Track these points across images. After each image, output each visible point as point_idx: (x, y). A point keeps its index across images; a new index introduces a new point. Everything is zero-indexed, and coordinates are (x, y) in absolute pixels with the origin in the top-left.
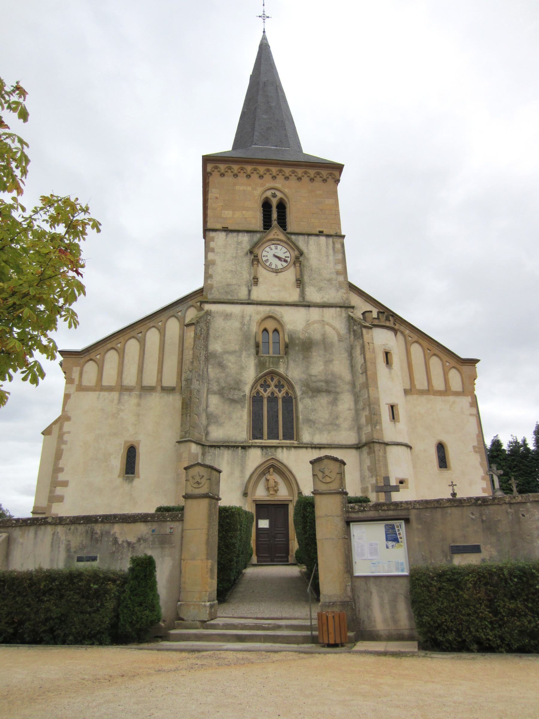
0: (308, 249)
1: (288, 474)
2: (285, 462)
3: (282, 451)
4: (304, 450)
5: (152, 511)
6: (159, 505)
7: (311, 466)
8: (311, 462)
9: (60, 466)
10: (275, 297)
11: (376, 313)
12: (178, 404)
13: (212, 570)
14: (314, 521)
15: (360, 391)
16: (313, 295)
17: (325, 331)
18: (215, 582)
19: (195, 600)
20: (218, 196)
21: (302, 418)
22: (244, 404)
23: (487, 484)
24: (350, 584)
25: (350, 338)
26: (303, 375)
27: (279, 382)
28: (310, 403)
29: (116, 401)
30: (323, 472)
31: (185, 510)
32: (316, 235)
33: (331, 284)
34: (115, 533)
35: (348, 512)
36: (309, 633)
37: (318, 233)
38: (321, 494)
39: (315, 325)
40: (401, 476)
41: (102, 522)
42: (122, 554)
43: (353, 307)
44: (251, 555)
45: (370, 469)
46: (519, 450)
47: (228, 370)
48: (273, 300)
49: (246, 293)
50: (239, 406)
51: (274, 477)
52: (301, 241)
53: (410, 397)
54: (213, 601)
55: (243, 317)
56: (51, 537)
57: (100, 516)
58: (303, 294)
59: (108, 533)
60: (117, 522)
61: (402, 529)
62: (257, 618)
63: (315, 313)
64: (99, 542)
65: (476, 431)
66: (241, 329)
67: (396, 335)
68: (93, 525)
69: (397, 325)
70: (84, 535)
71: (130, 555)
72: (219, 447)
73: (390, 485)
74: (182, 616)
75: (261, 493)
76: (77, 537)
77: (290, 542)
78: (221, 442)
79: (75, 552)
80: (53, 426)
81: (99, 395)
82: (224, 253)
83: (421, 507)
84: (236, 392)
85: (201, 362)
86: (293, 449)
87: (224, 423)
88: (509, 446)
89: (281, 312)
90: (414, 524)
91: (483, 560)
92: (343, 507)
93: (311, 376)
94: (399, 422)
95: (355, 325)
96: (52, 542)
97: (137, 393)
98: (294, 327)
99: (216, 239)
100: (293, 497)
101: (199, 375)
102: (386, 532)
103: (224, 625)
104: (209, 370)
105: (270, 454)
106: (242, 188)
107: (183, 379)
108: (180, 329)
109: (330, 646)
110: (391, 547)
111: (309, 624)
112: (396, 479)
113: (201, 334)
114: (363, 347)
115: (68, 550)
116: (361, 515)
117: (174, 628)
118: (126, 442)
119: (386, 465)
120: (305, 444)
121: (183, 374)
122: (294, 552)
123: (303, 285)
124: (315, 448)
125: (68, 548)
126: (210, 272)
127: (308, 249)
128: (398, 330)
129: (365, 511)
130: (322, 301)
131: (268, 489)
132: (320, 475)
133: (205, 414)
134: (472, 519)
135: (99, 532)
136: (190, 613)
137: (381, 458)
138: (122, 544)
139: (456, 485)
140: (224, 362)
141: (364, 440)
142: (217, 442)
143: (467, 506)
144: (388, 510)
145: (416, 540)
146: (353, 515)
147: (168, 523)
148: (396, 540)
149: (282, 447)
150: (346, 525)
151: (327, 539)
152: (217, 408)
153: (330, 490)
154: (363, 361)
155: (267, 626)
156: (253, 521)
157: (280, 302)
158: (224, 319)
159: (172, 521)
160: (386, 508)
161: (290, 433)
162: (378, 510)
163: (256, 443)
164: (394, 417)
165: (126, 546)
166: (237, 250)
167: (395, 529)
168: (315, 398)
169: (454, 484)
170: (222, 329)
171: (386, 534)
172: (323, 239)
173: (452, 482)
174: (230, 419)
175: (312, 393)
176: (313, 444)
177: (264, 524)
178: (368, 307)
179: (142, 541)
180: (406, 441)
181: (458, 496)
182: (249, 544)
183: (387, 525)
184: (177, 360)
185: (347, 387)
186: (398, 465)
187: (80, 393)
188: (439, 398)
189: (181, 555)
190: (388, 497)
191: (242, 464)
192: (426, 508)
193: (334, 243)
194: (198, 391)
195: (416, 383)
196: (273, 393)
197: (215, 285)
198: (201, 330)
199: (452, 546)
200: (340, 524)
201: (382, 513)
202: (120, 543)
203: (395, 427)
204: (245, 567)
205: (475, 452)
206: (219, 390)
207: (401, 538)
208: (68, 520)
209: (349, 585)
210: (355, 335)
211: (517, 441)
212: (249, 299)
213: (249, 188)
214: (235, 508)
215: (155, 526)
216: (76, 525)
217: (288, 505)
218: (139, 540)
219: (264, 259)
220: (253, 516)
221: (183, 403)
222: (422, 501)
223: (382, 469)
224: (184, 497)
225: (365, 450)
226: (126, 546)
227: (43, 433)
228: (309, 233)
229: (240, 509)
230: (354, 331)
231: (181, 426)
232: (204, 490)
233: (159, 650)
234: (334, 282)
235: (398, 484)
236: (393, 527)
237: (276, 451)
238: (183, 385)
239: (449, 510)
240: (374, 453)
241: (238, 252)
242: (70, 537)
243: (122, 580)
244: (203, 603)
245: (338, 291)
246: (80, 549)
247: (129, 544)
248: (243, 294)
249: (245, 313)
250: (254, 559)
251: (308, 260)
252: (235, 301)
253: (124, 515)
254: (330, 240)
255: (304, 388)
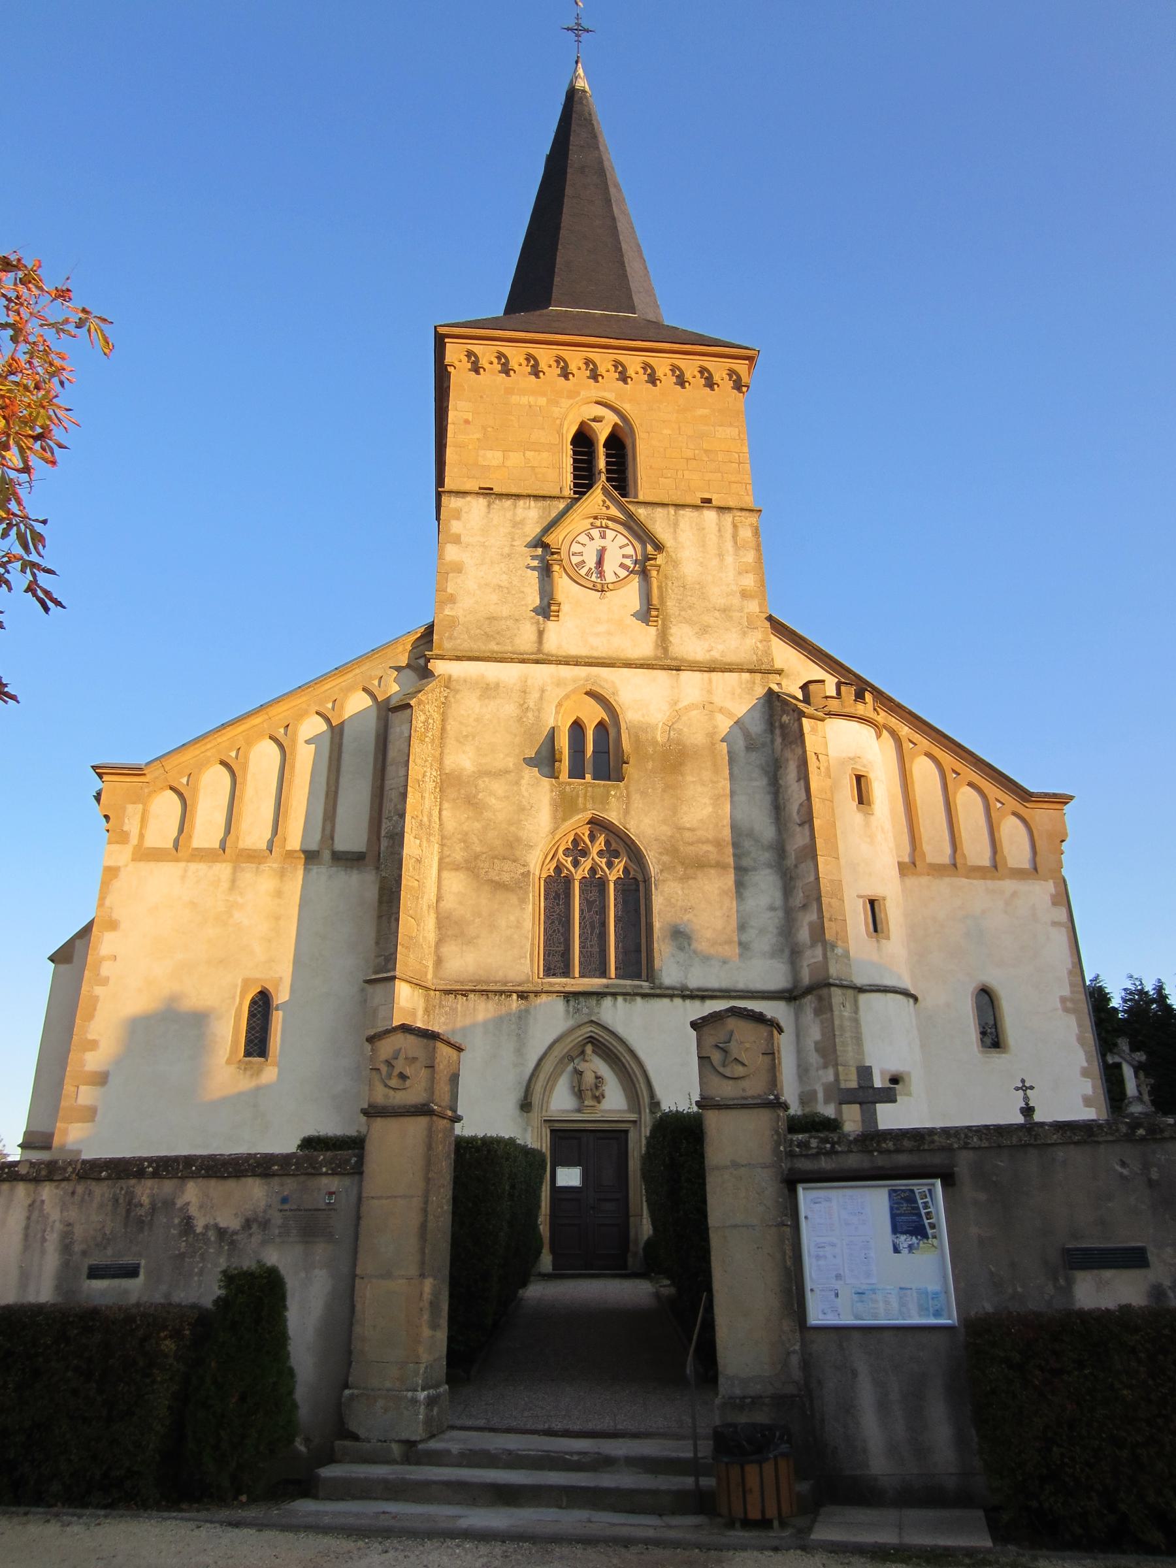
0: (675, 539)
1: (627, 1058)
2: (620, 1030)
3: (615, 1005)
4: (666, 1001)
5: (287, 1144)
6: (310, 1131)
7: (693, 1034)
8: (694, 1025)
9: (90, 1037)
10: (600, 647)
11: (834, 688)
12: (372, 893)
13: (434, 1305)
14: (704, 1179)
15: (796, 866)
16: (686, 643)
17: (715, 727)
18: (442, 1335)
19: (388, 1384)
20: (470, 417)
21: (661, 929)
22: (527, 893)
23: (1094, 1087)
24: (797, 1347)
25: (773, 741)
26: (664, 828)
27: (607, 843)
28: (680, 892)
29: (225, 885)
30: (725, 1051)
31: (369, 1146)
32: (695, 507)
33: (730, 618)
34: (188, 1204)
35: (791, 1155)
36: (688, 1482)
37: (699, 502)
38: (719, 1107)
39: (695, 712)
40: (894, 1067)
41: (155, 1175)
42: (203, 1258)
43: (779, 672)
44: (539, 1253)
45: (821, 1049)
46: (1148, 1009)
47: (487, 814)
48: (595, 654)
49: (533, 637)
50: (514, 899)
51: (598, 1066)
52: (658, 523)
53: (911, 881)
54: (437, 1386)
55: (525, 692)
56: (25, 1214)
57: (151, 1160)
58: (663, 639)
59: (169, 1204)
60: (194, 1176)
61: (935, 1198)
62: (550, 1433)
63: (692, 684)
64: (146, 1228)
65: (1067, 962)
66: (520, 719)
67: (879, 736)
68: (133, 1182)
69: (882, 714)
70: (109, 1208)
71: (223, 1263)
72: (465, 994)
73: (872, 1087)
74: (353, 1426)
75: (561, 1102)
76: (91, 1214)
77: (632, 1219)
78: (471, 981)
79: (84, 1253)
80: (78, 942)
81: (186, 871)
82: (483, 545)
83: (985, 1144)
84: (507, 865)
85: (427, 795)
86: (639, 999)
87: (478, 937)
88: (1125, 1001)
89: (613, 682)
90: (968, 1190)
91: (1157, 1292)
92: (778, 1144)
93: (680, 829)
94: (888, 938)
95: (784, 712)
96: (27, 1228)
97: (275, 865)
98: (643, 716)
99: (464, 516)
100: (640, 1113)
101: (421, 824)
102: (892, 1209)
103: (462, 1454)
104: (444, 813)
105: (585, 1010)
106: (524, 400)
107: (383, 833)
108: (378, 718)
109: (748, 1524)
110: (906, 1251)
111: (690, 1455)
112: (882, 1073)
113: (427, 730)
114: (803, 763)
115: (66, 1247)
116: (825, 1164)
117: (331, 1459)
118: (247, 982)
119: (858, 1039)
120: (668, 988)
121: (384, 821)
122: (642, 1244)
123: (664, 620)
124: (692, 997)
125: (67, 1241)
126: (449, 590)
127: (675, 539)
128: (885, 726)
129: (837, 1153)
130: (708, 657)
131: (579, 1093)
132: (716, 1057)
133: (433, 916)
134: (1121, 1175)
135: (145, 1200)
136: (371, 1421)
137: (847, 1023)
138: (203, 1234)
139: (1032, 1088)
140: (480, 796)
141: (806, 978)
142: (462, 983)
143: (1107, 1142)
144: (898, 1151)
145: (974, 1230)
146: (804, 1165)
147: (325, 1180)
148: (919, 1231)
149: (614, 995)
150: (786, 1191)
151: (735, 1226)
152: (460, 903)
153: (746, 1098)
154: (804, 797)
155: (575, 1458)
156: (545, 1171)
157: (610, 658)
158: (481, 698)
159: (334, 1174)
160: (890, 1145)
161: (637, 961)
162: (871, 1152)
163: (551, 984)
164: (876, 925)
165: (213, 1239)
166: (513, 540)
167: (916, 1202)
168: (690, 882)
169: (1027, 1085)
170: (477, 720)
171: (893, 1217)
172: (710, 515)
173: (1023, 1081)
174: (492, 927)
175: (686, 868)
176: (688, 989)
177: (569, 1177)
178: (815, 672)
179: (255, 1227)
180: (907, 983)
181: (1038, 1117)
182: (535, 1226)
183: (895, 1191)
184: (369, 789)
185: (766, 856)
186: (886, 1041)
187: (142, 864)
188: (979, 884)
189: (354, 1265)
190: (870, 1117)
191: (518, 1035)
192: (999, 1146)
193: (735, 526)
194: (419, 861)
195: (927, 847)
196: (593, 870)
197: (462, 620)
198: (426, 721)
199: (1069, 1250)
200: (766, 1183)
201: (881, 1161)
202: (199, 1230)
203: (879, 949)
204: (524, 1284)
205: (1066, 1010)
206: (466, 861)
207: (933, 1226)
208: (70, 1169)
209: (794, 1352)
210: (784, 736)
211: (1142, 989)
212: (539, 651)
213: (542, 401)
214: (498, 1141)
215: (290, 1185)
216: (89, 1182)
217: (626, 1132)
218: (248, 1224)
219: (575, 560)
220: (544, 1161)
221: (381, 889)
222: (987, 1127)
223: (850, 1048)
224: (365, 1112)
225: (809, 1002)
226: (213, 1239)
227: (51, 959)
228: (678, 502)
229: (511, 1141)
230: (783, 726)
231: (377, 943)
232: (413, 1095)
233: (285, 1528)
234: (736, 615)
235: (889, 1085)
236: (910, 1198)
237: (598, 1003)
238: (382, 848)
239: (1060, 1154)
240: (831, 1010)
241: (515, 543)
242: (73, 1214)
243: (203, 1324)
244: (410, 1394)
245: (744, 634)
246: (97, 1245)
247: (222, 1233)
248: (525, 638)
249: (529, 682)
250: (546, 1261)
251: (676, 564)
252: (506, 656)
253: (211, 1157)
254: (728, 518)
255: (665, 858)
